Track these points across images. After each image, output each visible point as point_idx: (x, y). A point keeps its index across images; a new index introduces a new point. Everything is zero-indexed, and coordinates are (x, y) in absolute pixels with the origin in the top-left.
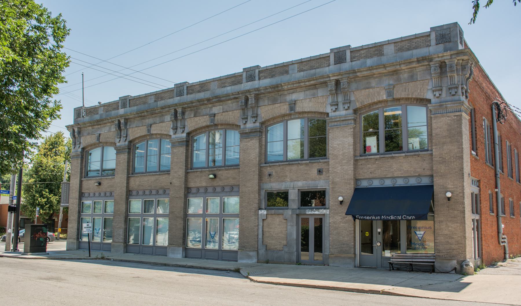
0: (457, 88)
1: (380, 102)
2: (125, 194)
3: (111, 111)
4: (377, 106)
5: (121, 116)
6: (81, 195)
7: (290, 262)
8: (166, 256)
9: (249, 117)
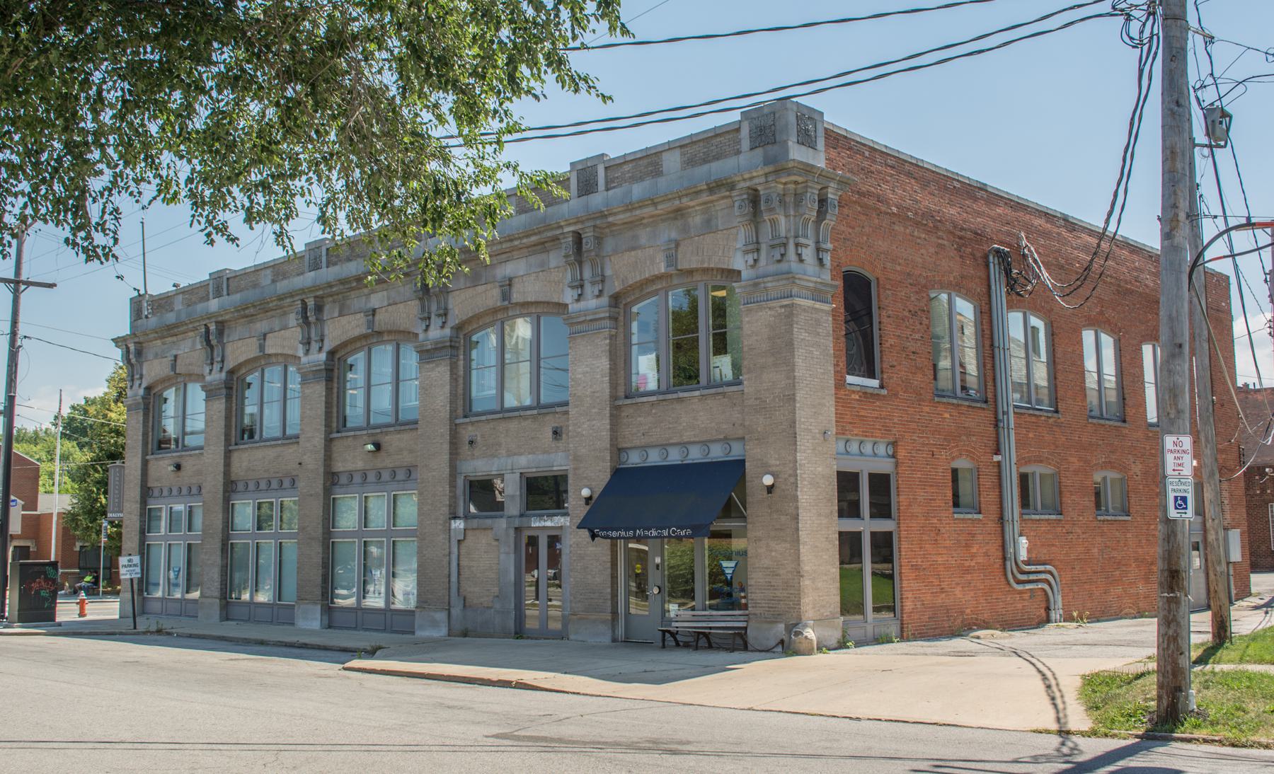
0: (785, 245)
1: (659, 278)
2: (221, 489)
3: (195, 303)
4: (654, 287)
5: (210, 316)
6: (146, 492)
7: (505, 635)
8: (293, 624)
9: (433, 317)
